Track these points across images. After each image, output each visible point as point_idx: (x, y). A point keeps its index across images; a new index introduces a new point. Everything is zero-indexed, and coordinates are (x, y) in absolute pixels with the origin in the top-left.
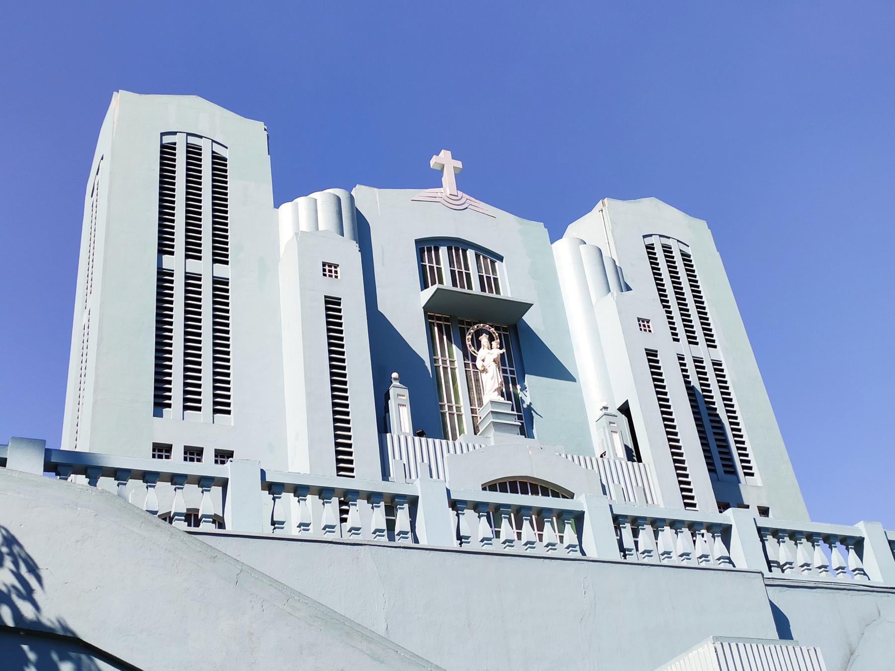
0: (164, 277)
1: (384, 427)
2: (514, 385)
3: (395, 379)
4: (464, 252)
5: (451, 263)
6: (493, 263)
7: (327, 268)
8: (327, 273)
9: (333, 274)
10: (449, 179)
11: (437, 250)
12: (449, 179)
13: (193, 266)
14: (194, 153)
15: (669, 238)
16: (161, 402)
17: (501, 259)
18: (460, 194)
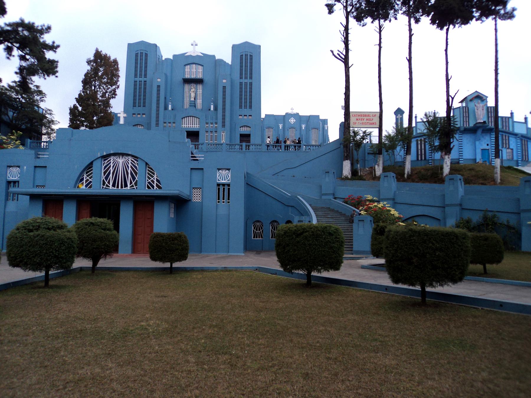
14: (246, 55)
16: (134, 105)
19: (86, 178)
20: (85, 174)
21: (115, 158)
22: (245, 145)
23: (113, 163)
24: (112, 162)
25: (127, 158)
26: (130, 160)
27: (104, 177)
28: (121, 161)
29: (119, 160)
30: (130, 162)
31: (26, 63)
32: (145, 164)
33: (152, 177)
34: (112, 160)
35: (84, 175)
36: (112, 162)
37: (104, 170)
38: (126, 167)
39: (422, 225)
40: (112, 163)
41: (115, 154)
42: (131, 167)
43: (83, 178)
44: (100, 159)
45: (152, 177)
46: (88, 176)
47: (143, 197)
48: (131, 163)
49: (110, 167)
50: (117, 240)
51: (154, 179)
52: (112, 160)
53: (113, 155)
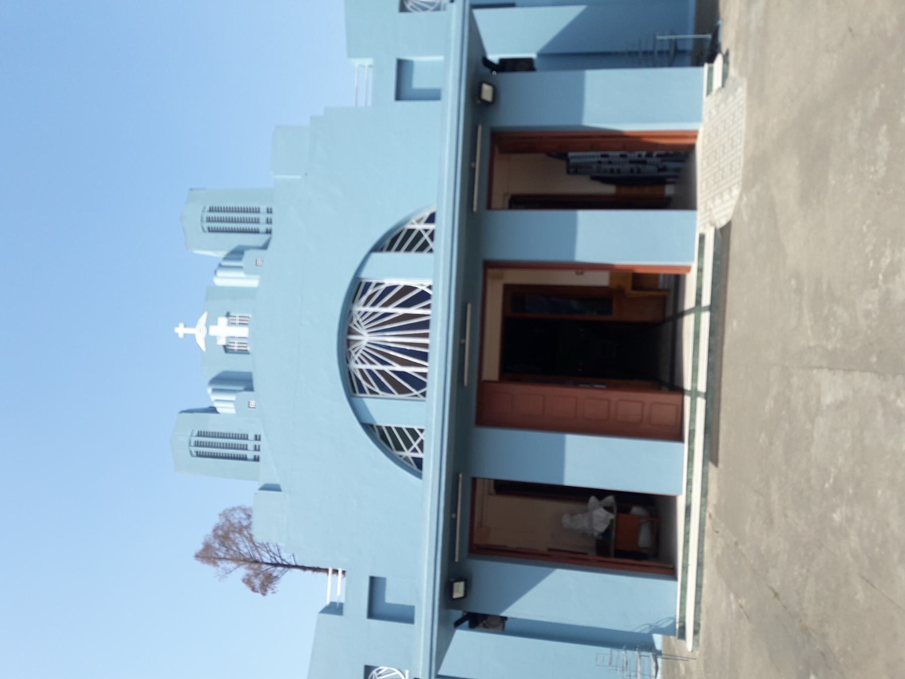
13: (251, 447)
14: (197, 444)
19: (415, 451)
20: (401, 453)
21: (356, 358)
22: (420, 284)
23: (371, 363)
24: (369, 366)
25: (358, 317)
26: (363, 309)
27: (415, 392)
28: (365, 338)
29: (364, 343)
30: (371, 310)
31: (213, 539)
32: (375, 256)
33: (420, 235)
34: (361, 366)
35: (406, 459)
36: (369, 366)
37: (391, 392)
38: (380, 323)
39: (461, 476)
40: (373, 367)
41: (344, 356)
42: (386, 305)
43: (414, 458)
44: (354, 399)
45: (420, 235)
46: (409, 445)
47: (455, 520)
48: (374, 305)
49: (382, 372)
50: (279, 576)
51: (426, 230)
52: (361, 366)
53: (348, 362)
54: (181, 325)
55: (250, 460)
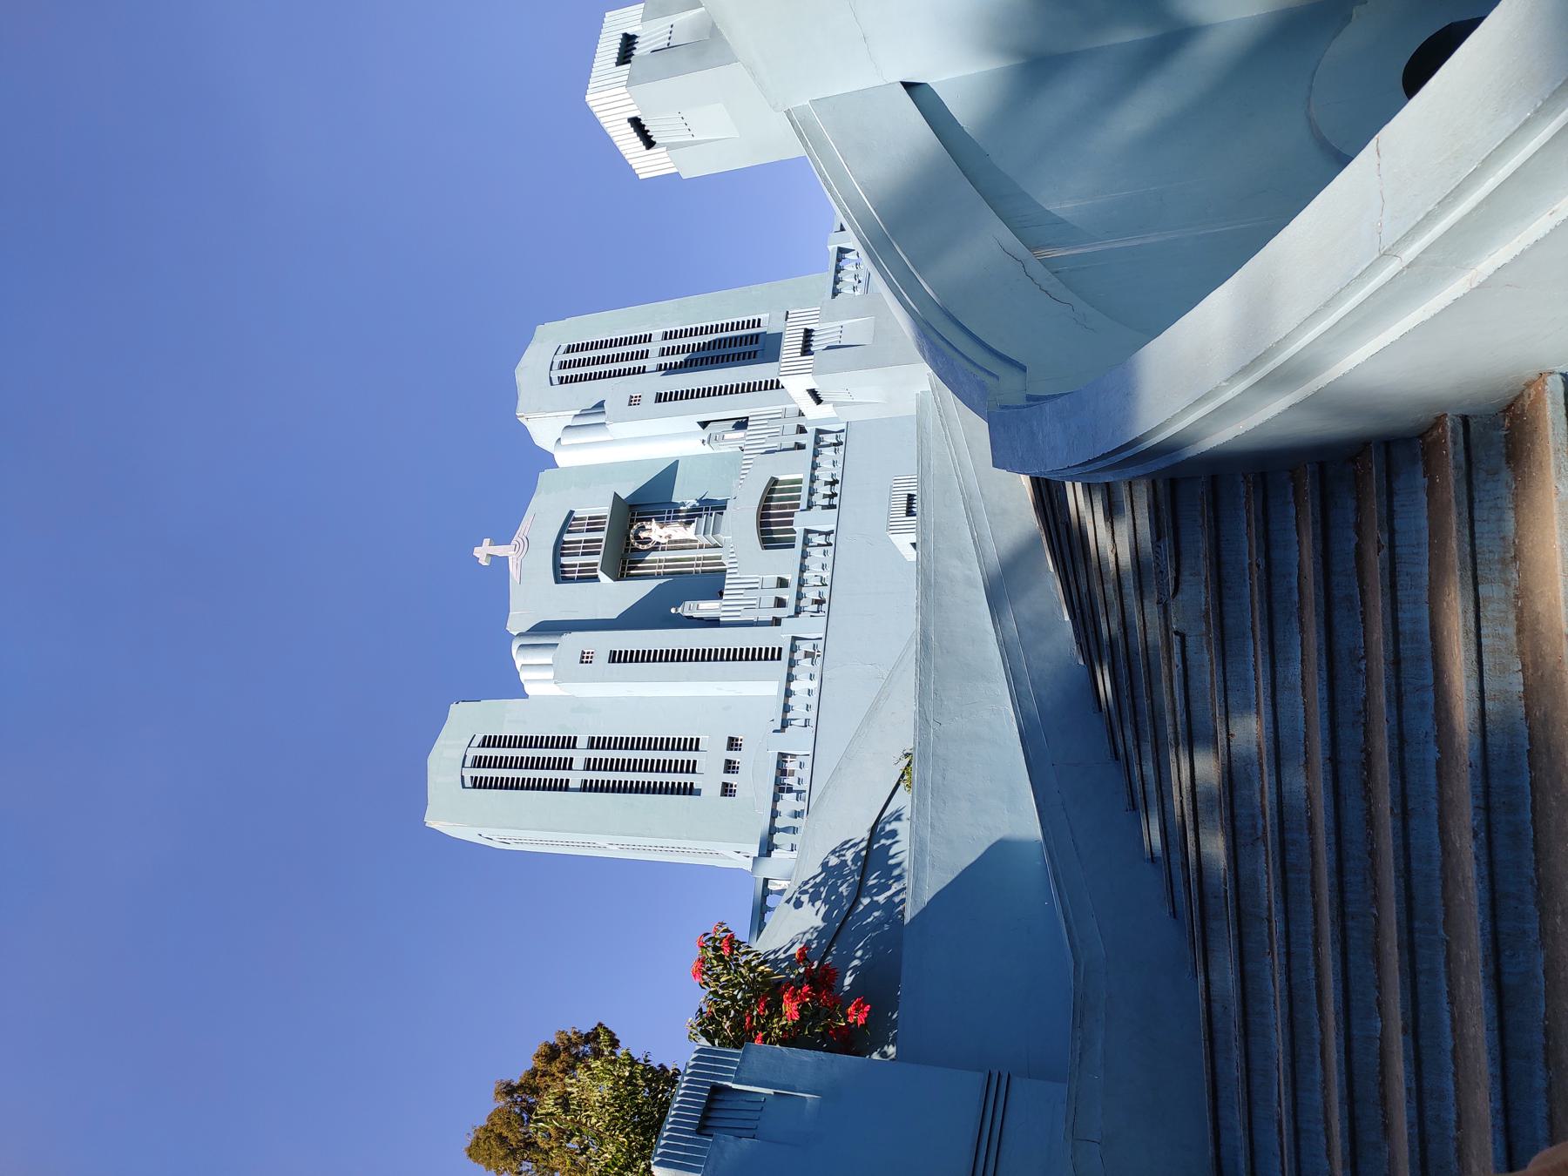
0: (587, 787)
1: (714, 623)
2: (680, 511)
3: (676, 610)
4: (565, 543)
5: (576, 555)
6: (575, 519)
7: (585, 660)
8: (589, 660)
9: (590, 655)
10: (499, 551)
11: (563, 566)
12: (499, 551)
13: (578, 763)
14: (479, 762)
15: (552, 362)
17: (572, 512)
18: (514, 542)
54: (487, 541)
55: (575, 790)
